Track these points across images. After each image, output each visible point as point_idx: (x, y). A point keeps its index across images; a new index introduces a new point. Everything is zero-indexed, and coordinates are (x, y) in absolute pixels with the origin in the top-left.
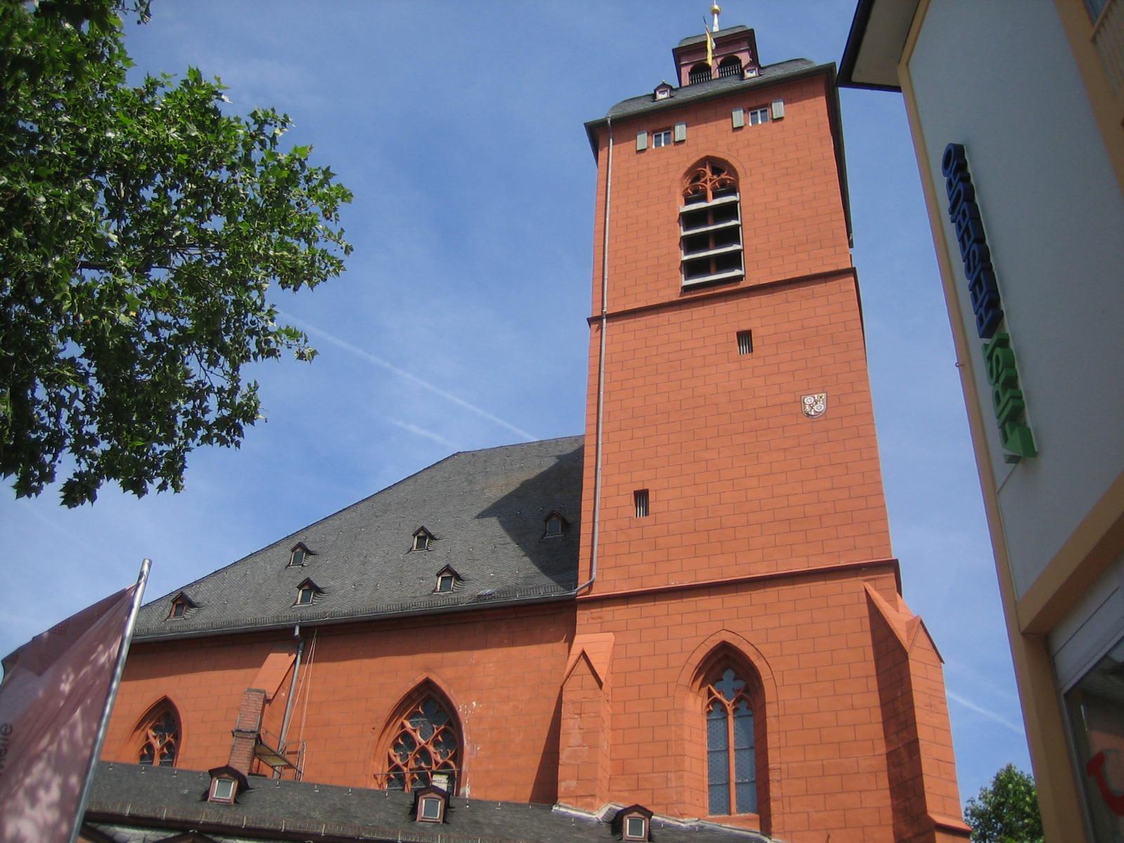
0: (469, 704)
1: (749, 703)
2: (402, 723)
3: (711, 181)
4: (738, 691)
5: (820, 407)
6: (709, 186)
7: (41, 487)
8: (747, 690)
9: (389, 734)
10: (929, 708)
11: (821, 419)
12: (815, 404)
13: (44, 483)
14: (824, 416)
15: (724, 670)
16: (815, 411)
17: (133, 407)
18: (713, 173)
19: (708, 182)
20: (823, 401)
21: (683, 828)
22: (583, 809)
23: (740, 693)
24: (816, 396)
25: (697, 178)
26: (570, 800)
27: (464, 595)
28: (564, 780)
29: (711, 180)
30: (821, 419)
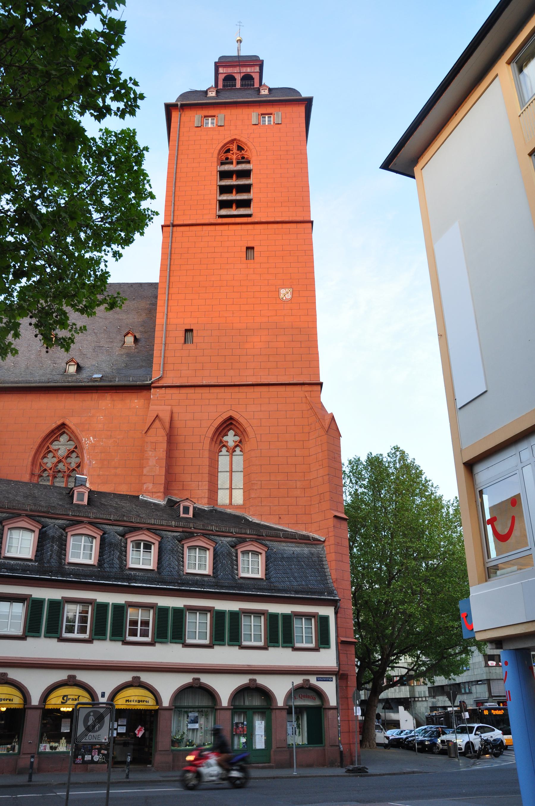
0: (89, 439)
1: (242, 448)
2: (48, 446)
3: (236, 155)
4: (236, 442)
5: (289, 296)
6: (234, 157)
7: (86, 17)
8: (240, 441)
9: (40, 452)
10: (333, 459)
11: (289, 302)
12: (285, 294)
13: (86, 14)
14: (285, 302)
15: (229, 430)
16: (286, 298)
17: (394, 656)
18: (238, 150)
19: (235, 154)
20: (291, 293)
21: (206, 510)
22: (156, 499)
23: (237, 443)
24: (287, 289)
25: (228, 151)
26: (149, 494)
27: (84, 378)
28: (387, 695)
29: (236, 154)
30: (289, 302)
